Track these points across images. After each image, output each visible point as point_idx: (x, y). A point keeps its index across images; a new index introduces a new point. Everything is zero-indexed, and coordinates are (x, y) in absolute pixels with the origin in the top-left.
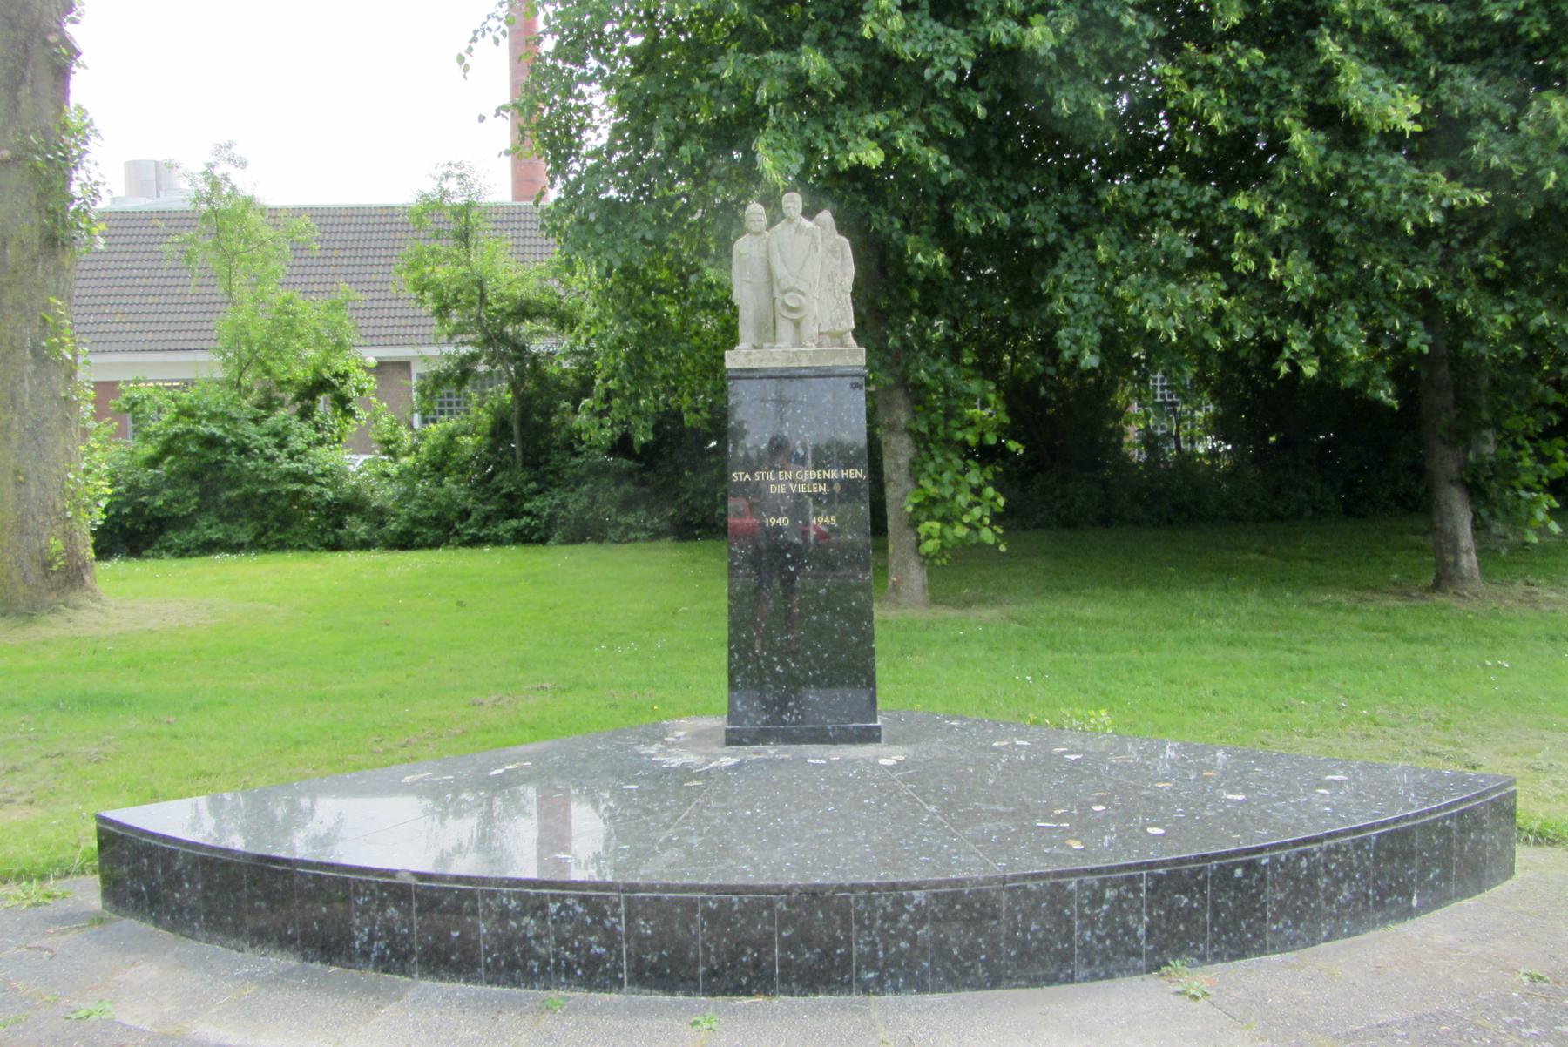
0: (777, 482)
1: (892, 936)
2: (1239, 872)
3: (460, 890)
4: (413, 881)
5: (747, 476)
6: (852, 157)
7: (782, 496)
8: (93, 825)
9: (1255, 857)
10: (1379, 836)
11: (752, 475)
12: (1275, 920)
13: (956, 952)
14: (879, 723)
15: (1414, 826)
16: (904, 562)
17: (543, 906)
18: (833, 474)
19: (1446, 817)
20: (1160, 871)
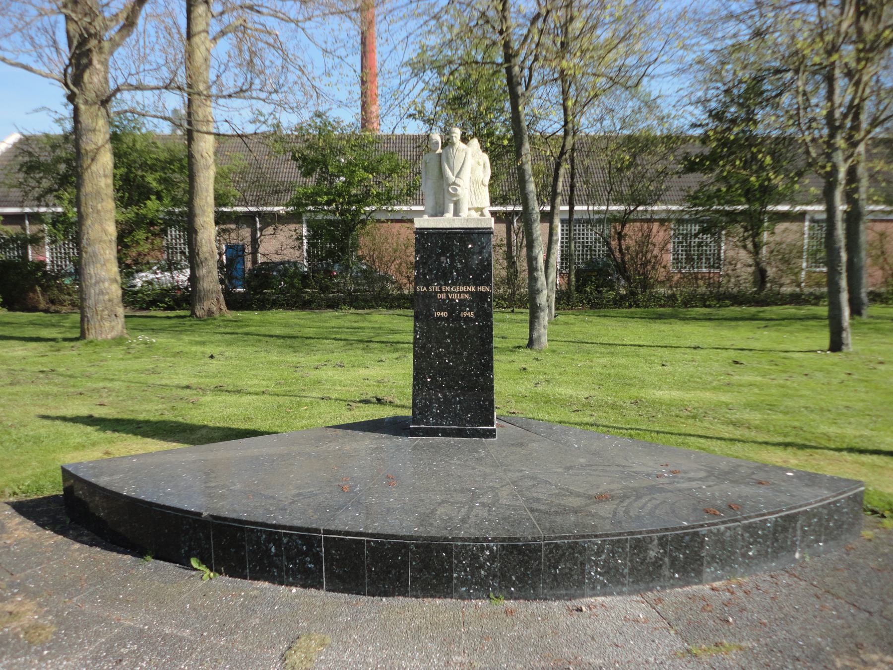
0: (441, 292)
1: (476, 568)
2: (687, 538)
3: (210, 549)
4: (210, 519)
5: (425, 289)
6: (103, 336)
7: (445, 300)
8: (60, 472)
9: (698, 530)
10: (776, 518)
11: (428, 288)
12: (709, 566)
13: (514, 578)
14: (495, 427)
15: (799, 513)
16: (885, 38)
17: (280, 539)
18: (472, 289)
19: (820, 506)
20: (639, 536)
